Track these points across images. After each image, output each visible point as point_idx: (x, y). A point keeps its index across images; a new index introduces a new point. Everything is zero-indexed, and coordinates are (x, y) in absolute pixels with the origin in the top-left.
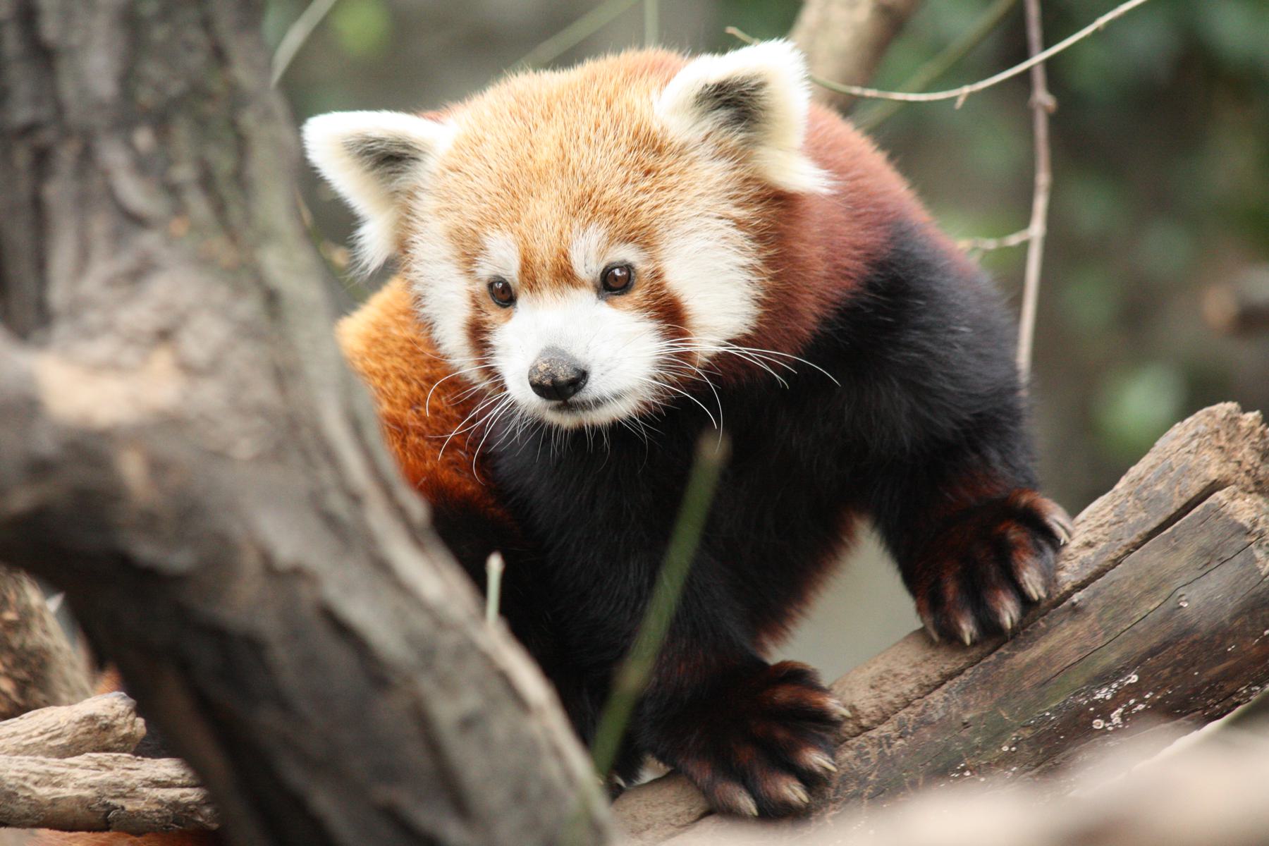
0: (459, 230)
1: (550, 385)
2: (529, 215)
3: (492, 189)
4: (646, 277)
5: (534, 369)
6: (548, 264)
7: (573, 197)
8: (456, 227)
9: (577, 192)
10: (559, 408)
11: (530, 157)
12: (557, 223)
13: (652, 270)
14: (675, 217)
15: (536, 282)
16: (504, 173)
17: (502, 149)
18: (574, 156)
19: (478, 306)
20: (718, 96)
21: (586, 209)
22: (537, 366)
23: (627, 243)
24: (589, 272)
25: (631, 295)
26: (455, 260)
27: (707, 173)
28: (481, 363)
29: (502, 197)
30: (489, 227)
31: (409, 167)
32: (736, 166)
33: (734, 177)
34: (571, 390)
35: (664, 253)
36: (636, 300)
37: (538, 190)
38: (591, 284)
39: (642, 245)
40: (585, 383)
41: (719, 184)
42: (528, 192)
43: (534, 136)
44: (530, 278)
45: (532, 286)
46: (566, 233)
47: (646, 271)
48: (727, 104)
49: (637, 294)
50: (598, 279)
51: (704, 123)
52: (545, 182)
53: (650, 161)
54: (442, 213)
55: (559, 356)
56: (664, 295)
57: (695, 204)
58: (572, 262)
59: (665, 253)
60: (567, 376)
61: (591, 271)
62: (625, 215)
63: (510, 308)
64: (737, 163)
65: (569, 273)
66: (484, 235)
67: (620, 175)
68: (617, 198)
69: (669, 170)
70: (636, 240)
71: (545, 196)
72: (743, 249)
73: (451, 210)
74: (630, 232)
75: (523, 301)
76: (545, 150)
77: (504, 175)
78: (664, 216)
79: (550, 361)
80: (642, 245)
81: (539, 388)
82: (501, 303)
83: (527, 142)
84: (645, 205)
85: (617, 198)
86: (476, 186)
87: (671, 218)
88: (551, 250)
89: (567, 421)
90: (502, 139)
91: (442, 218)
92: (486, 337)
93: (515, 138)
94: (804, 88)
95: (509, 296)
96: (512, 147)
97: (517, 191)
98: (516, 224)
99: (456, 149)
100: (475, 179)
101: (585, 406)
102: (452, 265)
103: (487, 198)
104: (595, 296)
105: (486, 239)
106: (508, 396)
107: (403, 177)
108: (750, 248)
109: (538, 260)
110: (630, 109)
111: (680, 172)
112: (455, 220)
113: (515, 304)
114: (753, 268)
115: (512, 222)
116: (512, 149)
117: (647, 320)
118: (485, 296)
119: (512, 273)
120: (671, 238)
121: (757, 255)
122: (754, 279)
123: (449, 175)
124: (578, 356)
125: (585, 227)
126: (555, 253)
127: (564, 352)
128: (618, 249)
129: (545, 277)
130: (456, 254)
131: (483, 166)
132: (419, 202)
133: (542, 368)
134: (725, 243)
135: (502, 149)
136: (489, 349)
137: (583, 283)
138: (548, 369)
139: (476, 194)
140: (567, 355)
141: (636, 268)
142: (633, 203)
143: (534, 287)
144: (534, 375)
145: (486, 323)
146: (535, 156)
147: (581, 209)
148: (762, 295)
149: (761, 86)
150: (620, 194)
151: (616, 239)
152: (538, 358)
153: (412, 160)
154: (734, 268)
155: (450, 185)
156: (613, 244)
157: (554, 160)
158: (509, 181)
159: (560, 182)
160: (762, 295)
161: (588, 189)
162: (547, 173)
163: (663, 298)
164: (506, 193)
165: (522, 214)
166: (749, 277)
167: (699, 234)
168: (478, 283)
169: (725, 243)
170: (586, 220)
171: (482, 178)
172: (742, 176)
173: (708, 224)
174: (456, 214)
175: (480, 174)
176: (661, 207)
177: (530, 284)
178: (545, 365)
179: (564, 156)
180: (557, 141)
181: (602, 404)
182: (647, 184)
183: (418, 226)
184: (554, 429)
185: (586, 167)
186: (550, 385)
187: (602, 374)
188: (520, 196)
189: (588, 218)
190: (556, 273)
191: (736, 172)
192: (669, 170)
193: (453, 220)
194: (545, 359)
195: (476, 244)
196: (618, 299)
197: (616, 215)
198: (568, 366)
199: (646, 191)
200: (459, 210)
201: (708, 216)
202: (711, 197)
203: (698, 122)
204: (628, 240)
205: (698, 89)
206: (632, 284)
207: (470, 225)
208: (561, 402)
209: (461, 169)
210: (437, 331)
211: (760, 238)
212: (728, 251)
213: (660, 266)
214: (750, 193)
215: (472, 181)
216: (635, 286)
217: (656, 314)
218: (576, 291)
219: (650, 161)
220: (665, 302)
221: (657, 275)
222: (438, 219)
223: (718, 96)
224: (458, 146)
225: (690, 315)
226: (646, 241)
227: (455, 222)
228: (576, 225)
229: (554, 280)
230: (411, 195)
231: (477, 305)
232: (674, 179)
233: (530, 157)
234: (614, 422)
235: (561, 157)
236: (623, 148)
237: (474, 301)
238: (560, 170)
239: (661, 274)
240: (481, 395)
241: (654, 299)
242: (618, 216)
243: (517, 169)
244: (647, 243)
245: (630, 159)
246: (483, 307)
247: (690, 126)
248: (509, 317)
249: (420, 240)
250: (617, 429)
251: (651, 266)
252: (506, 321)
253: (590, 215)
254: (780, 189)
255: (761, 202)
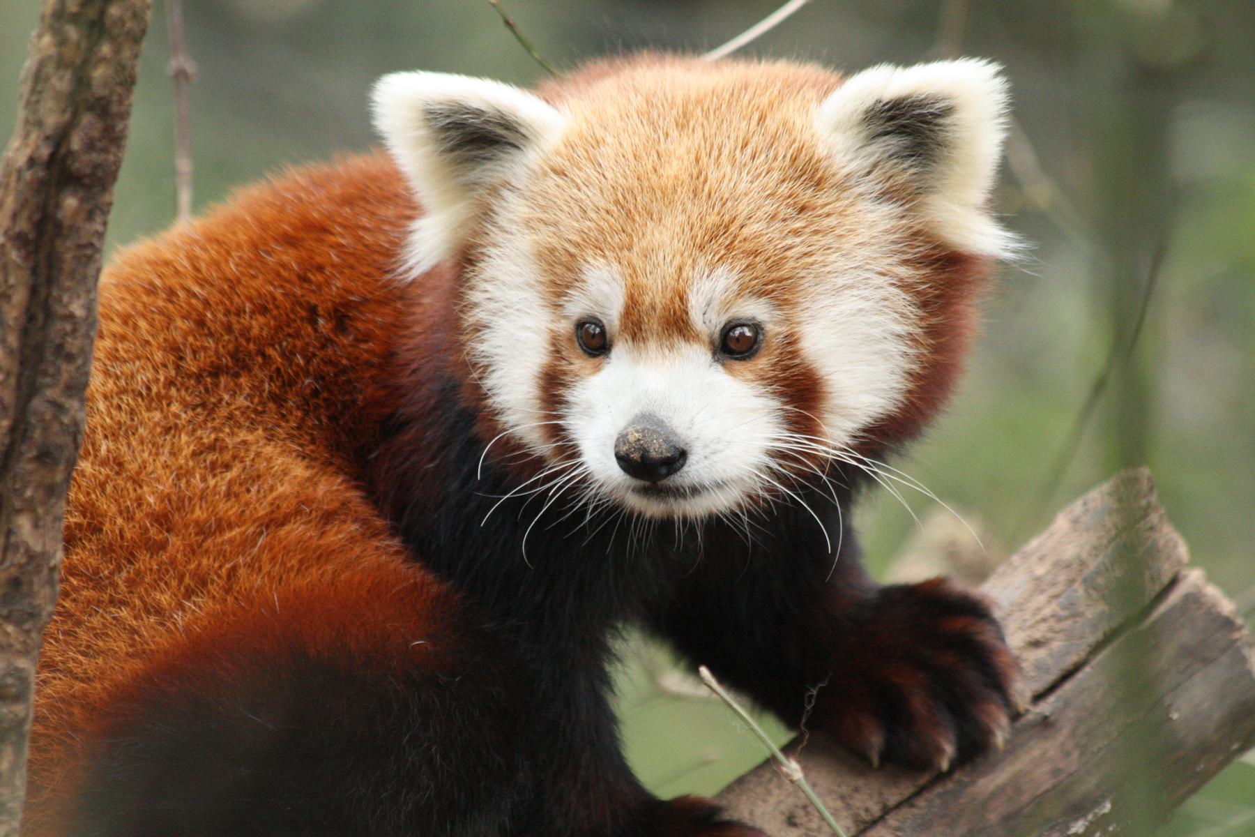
0: (552, 251)
1: (639, 461)
2: (644, 243)
3: (602, 204)
4: (776, 342)
5: (622, 439)
6: (659, 306)
7: (705, 226)
8: (549, 246)
9: (712, 219)
10: (644, 492)
11: (656, 171)
12: (678, 257)
13: (785, 334)
14: (827, 269)
15: (641, 329)
16: (621, 186)
17: (624, 156)
18: (713, 176)
19: (558, 351)
20: (891, 118)
21: (720, 242)
22: (627, 435)
23: (760, 297)
24: (707, 322)
25: (755, 362)
26: (540, 288)
27: (871, 217)
28: (548, 417)
29: (612, 216)
30: (590, 252)
31: (502, 155)
32: (904, 214)
33: (903, 227)
34: (663, 471)
35: (805, 316)
36: (761, 369)
37: (660, 212)
38: (707, 339)
39: (778, 302)
40: (682, 465)
41: (887, 232)
42: (648, 215)
43: (663, 146)
44: (635, 326)
45: (635, 334)
46: (687, 269)
47: (777, 334)
48: (901, 130)
49: (763, 362)
50: (717, 335)
51: (873, 148)
52: (670, 203)
53: (806, 196)
54: (532, 224)
55: (654, 427)
56: (797, 365)
57: (854, 254)
58: (689, 306)
59: (807, 315)
60: (662, 453)
61: (710, 321)
62: (767, 260)
63: (601, 358)
64: (906, 210)
65: (683, 321)
66: (582, 261)
67: (769, 208)
68: (761, 235)
69: (826, 210)
70: (773, 295)
71: (668, 221)
72: (902, 315)
73: (546, 224)
74: (767, 284)
75: (620, 352)
76: (675, 163)
77: (619, 188)
78: (814, 267)
79: (643, 431)
80: (778, 302)
81: (624, 461)
82: (585, 348)
83: (654, 153)
84: (793, 250)
85: (761, 235)
86: (584, 197)
87: (823, 269)
88: (664, 288)
89: (652, 508)
90: (625, 145)
91: (533, 231)
92: (562, 391)
93: (641, 147)
94: (999, 127)
95: (601, 342)
96: (635, 156)
97: (632, 209)
98: (626, 252)
99: (566, 146)
100: (584, 188)
101: (678, 493)
102: (535, 293)
103: (593, 215)
104: (709, 356)
105: (585, 267)
106: (582, 464)
107: (489, 165)
108: (912, 316)
109: (647, 300)
110: (786, 127)
111: (840, 214)
112: (549, 236)
113: (609, 353)
114: (912, 338)
115: (621, 249)
116: (635, 159)
117: (769, 395)
118: (570, 340)
119: (613, 315)
120: (818, 294)
121: (919, 322)
122: (911, 351)
123: (552, 178)
124: (679, 431)
125: (712, 267)
126: (669, 295)
127: (663, 422)
128: (747, 303)
129: (654, 324)
130: (542, 279)
131: (597, 175)
132: (505, 204)
133: (631, 438)
134: (884, 306)
135: (624, 156)
136: (564, 406)
137: (698, 335)
138: (639, 440)
139: (580, 207)
140: (666, 426)
141: (766, 329)
142: (780, 246)
143: (638, 335)
144: (621, 445)
145: (565, 373)
146: (661, 171)
147: (713, 241)
148: (916, 368)
149: (947, 111)
150: (764, 232)
151: (748, 291)
152: (629, 425)
153: (508, 147)
154: (888, 336)
155: (549, 191)
156: (742, 296)
157: (686, 177)
158: (625, 198)
159: (689, 205)
160: (916, 368)
161: (727, 218)
162: (675, 191)
163: (793, 370)
164: (619, 211)
165: (635, 240)
166: (904, 349)
167: (855, 292)
168: (563, 321)
169: (884, 306)
170: (717, 258)
171: (591, 188)
172: (911, 227)
173: (868, 278)
174: (552, 229)
175: (590, 183)
176: (812, 255)
177: (634, 330)
178: (637, 435)
179: (700, 173)
180: (692, 157)
181: (700, 492)
182: (798, 225)
183: (497, 236)
184: (635, 515)
185: (725, 190)
186: (639, 461)
187: (706, 457)
188: (637, 218)
189: (719, 256)
190: (668, 320)
191: (904, 221)
192: (826, 210)
193: (545, 236)
194: (638, 428)
195: (570, 274)
196: (738, 366)
197: (755, 257)
198: (665, 441)
199: (796, 233)
200: (556, 224)
201: (867, 270)
202: (873, 247)
203: (864, 146)
204: (762, 294)
205: (869, 102)
206: (757, 350)
207: (567, 245)
208: (647, 484)
209: (566, 173)
210: (495, 375)
211: (924, 305)
212: (885, 316)
213: (796, 330)
214: (920, 252)
215: (579, 190)
216: (762, 352)
217: (782, 389)
218: (688, 346)
219: (806, 196)
220: (795, 376)
221: (791, 341)
222: (527, 231)
223: (891, 118)
224: (570, 145)
225: (831, 393)
226: (786, 297)
227: (549, 239)
228: (702, 262)
229: (663, 328)
230: (494, 191)
231: (557, 352)
232: (832, 221)
233: (656, 171)
234: (711, 516)
235: (695, 176)
236: (776, 175)
237: (553, 345)
238: (691, 191)
239: (796, 340)
240: (539, 463)
241: (782, 369)
242: (758, 259)
243: (636, 183)
244: (786, 300)
245: (784, 189)
246: (564, 353)
247: (857, 147)
248: (597, 369)
249: (499, 256)
250: (717, 525)
251: (784, 329)
252: (594, 373)
253: (723, 252)
254: (954, 249)
255: (932, 264)
